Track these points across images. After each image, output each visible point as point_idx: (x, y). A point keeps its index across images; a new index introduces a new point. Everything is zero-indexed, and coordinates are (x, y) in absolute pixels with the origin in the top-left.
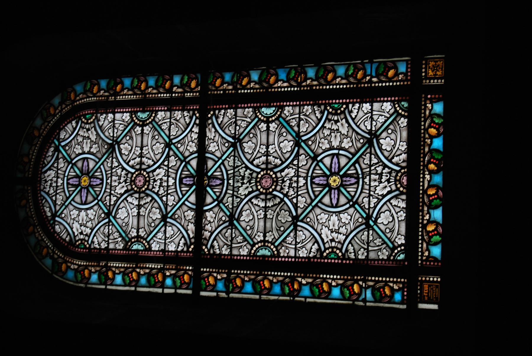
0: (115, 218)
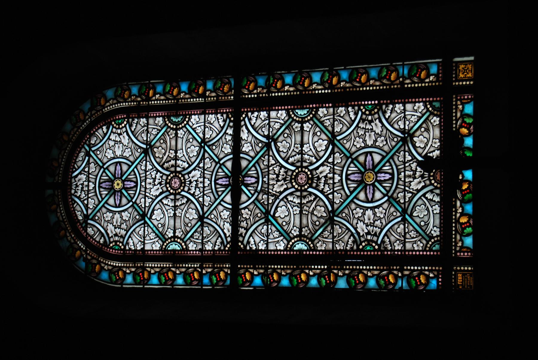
0: (411, 216)
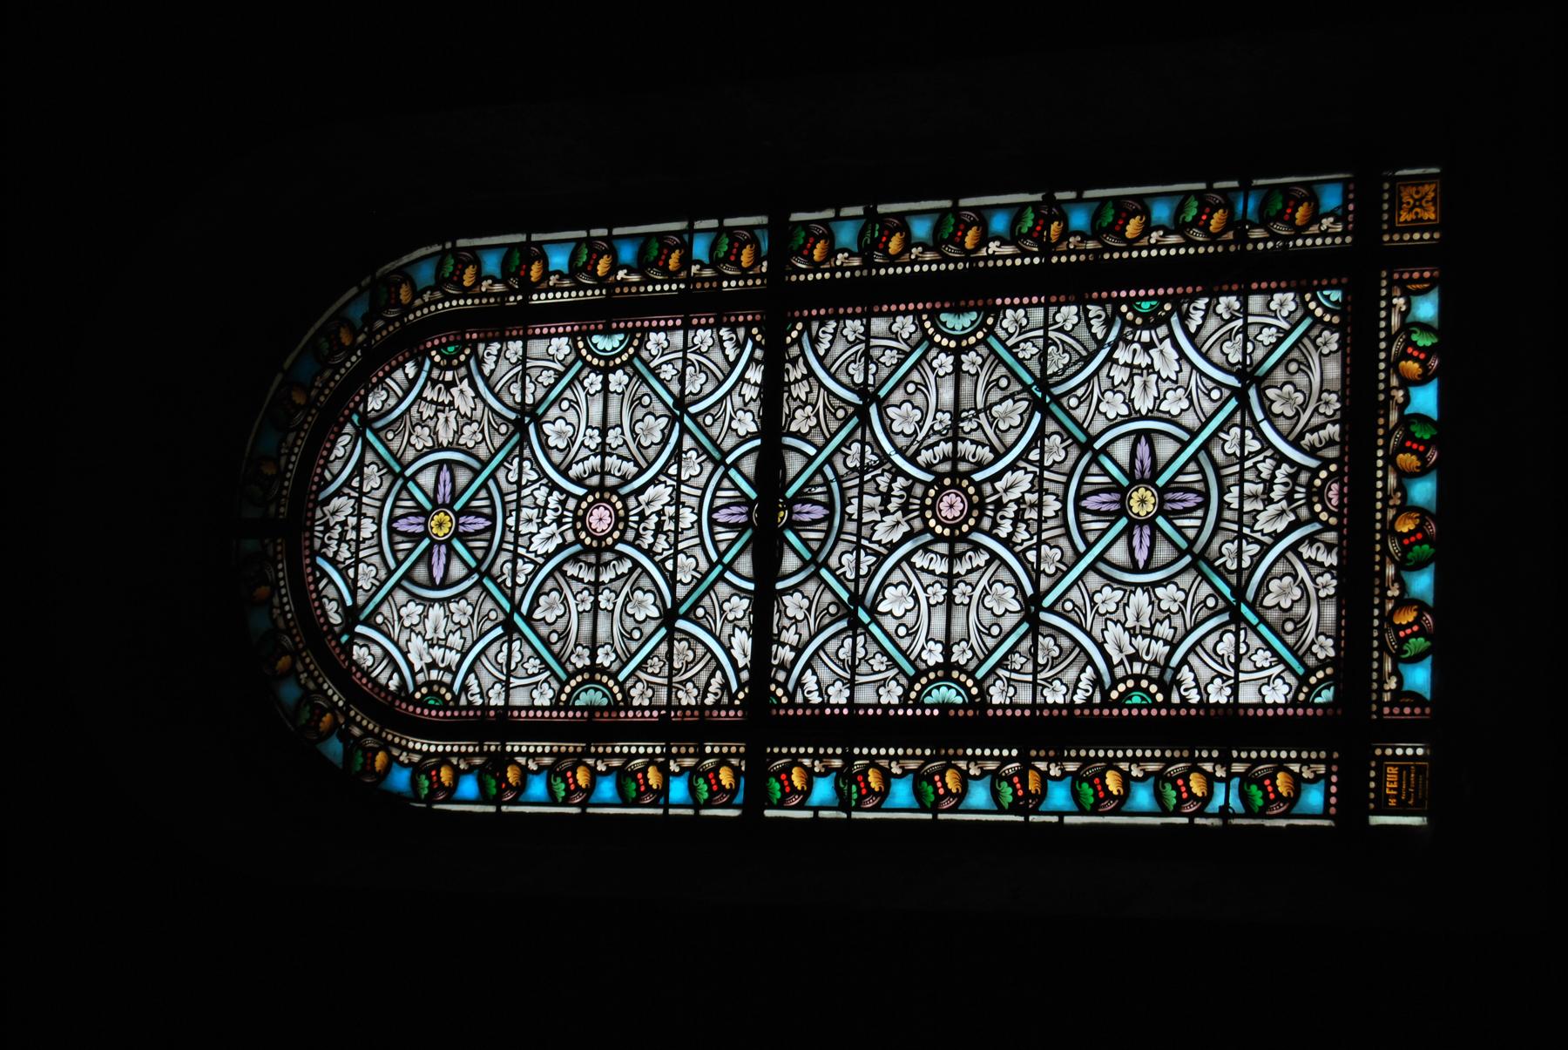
0: (872, 611)
